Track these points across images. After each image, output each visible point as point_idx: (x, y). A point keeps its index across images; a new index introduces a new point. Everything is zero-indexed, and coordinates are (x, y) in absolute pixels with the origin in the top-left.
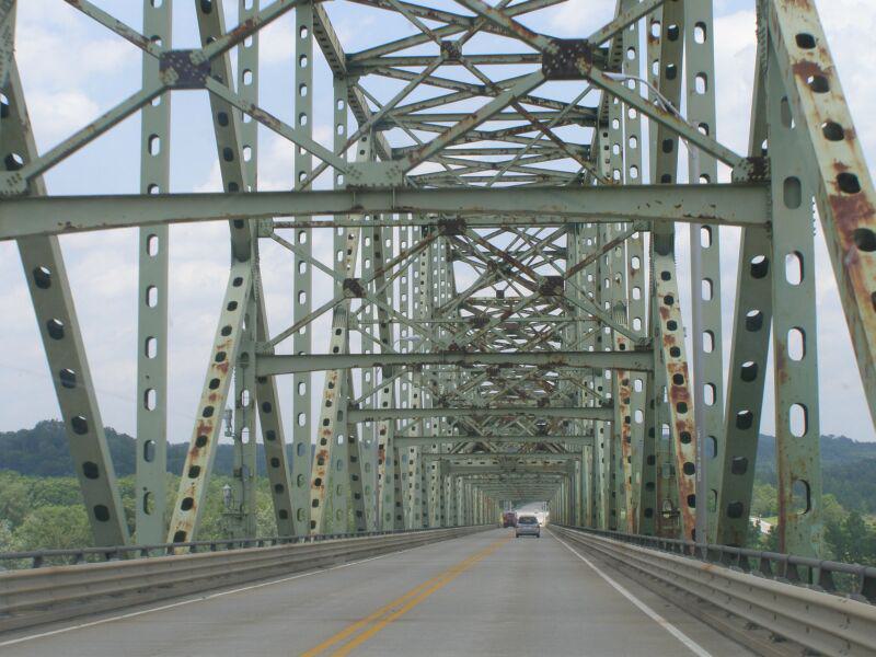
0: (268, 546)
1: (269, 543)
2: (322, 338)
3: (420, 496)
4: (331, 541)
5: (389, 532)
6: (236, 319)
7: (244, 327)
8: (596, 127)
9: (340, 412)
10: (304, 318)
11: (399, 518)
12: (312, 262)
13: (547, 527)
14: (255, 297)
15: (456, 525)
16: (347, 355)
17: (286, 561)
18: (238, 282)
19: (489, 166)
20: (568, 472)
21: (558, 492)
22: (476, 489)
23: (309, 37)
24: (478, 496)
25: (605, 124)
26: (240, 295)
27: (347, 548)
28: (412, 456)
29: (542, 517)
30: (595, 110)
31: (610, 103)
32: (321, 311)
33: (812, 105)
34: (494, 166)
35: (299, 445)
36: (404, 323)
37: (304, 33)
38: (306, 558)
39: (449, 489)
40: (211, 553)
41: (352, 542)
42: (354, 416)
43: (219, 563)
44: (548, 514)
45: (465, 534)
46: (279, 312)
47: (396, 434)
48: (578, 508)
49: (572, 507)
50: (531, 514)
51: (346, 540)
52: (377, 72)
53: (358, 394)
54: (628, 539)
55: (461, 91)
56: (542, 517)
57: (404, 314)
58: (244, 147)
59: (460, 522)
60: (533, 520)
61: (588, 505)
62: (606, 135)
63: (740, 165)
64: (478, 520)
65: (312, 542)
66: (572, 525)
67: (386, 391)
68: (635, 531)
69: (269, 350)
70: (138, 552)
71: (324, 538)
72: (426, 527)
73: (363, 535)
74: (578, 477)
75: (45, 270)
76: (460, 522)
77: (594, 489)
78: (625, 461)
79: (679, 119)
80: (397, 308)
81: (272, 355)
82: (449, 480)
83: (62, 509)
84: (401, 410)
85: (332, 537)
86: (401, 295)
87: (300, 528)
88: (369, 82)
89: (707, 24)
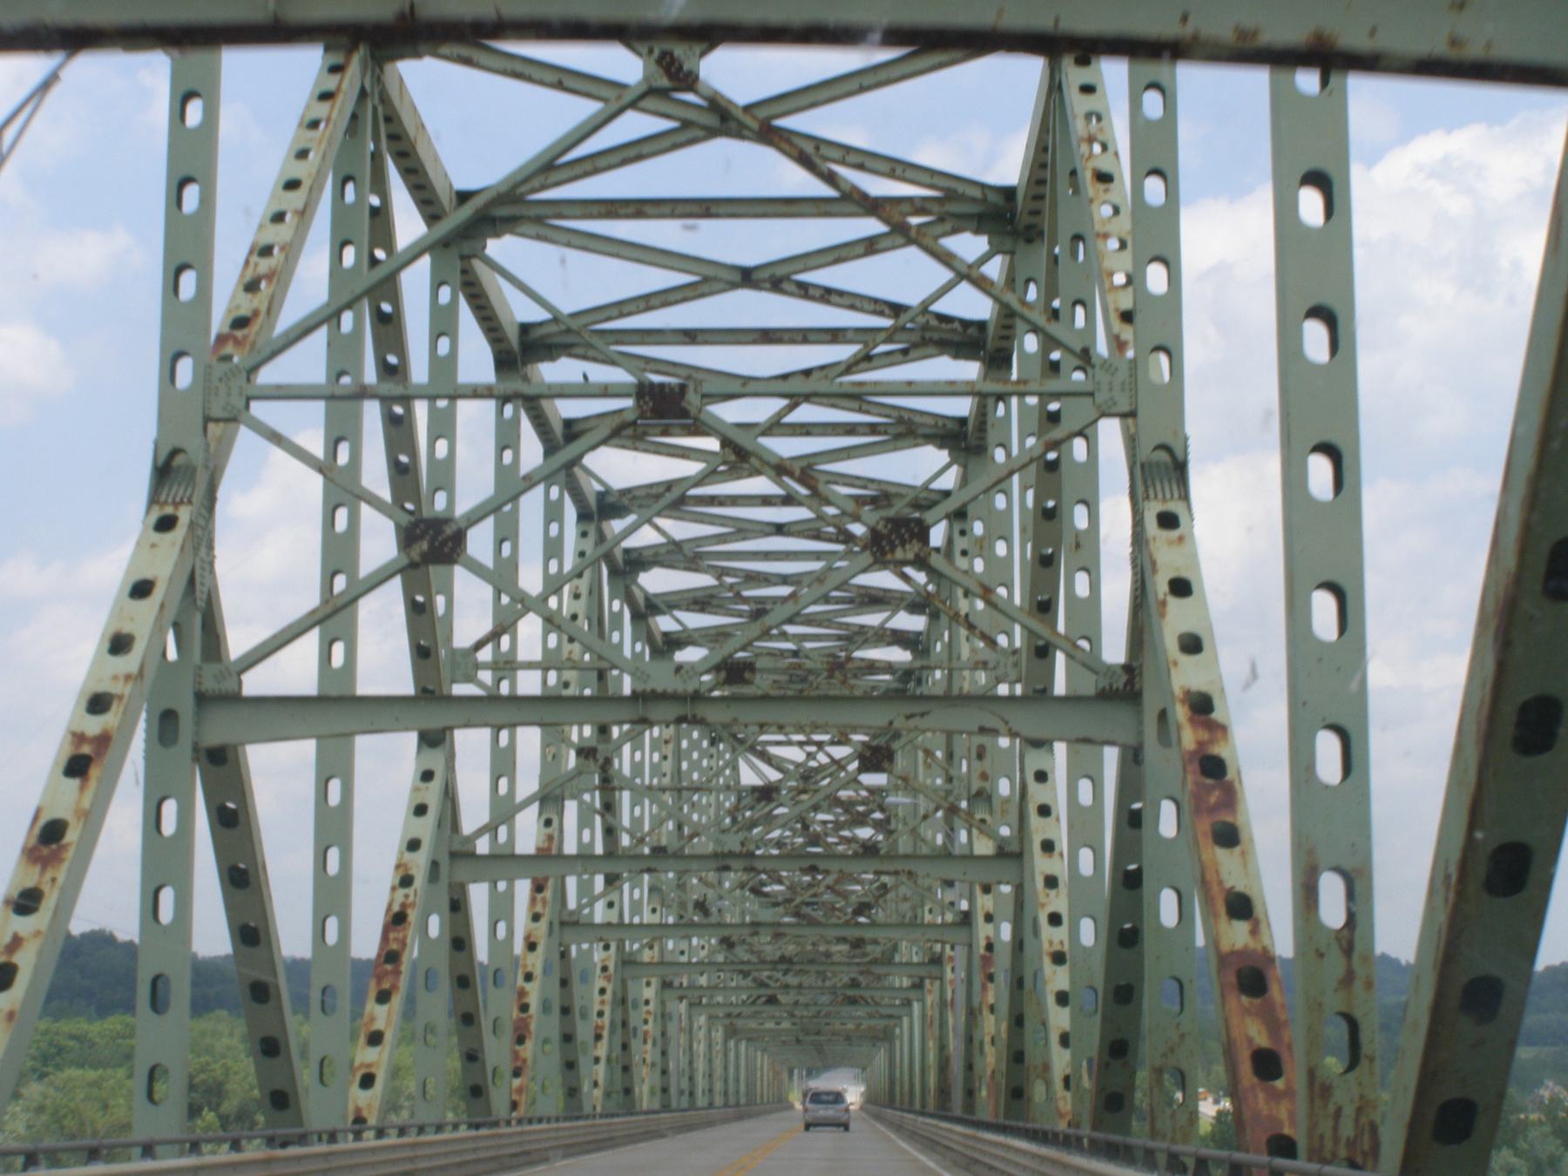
0: (463, 1132)
1: (394, 1132)
2: (527, 833)
3: (658, 1059)
4: (544, 1126)
5: (654, 1112)
6: (425, 828)
7: (172, 654)
8: (983, 360)
9: (435, 865)
10: (504, 810)
11: (628, 1091)
12: (325, 468)
13: (862, 1108)
14: (450, 795)
15: (711, 1105)
16: (560, 856)
17: (590, 1138)
18: (427, 776)
19: (772, 529)
20: (885, 1037)
21: (877, 1058)
22: (759, 1053)
23: (454, 300)
24: (763, 1061)
25: (997, 360)
26: (432, 794)
27: (475, 1150)
28: (649, 993)
29: (854, 1095)
30: (1009, 193)
31: (990, 415)
32: (527, 803)
33: (1177, 618)
34: (784, 580)
35: (427, 972)
36: (639, 794)
37: (445, 294)
38: (581, 1131)
39: (732, 1055)
40: (235, 1157)
41: (558, 1129)
42: (462, 870)
43: (365, 1160)
44: (863, 1089)
45: (750, 1116)
46: (474, 812)
47: (566, 918)
48: (898, 1084)
49: (892, 1082)
50: (839, 1088)
51: (519, 1129)
52: (571, 355)
53: (572, 904)
54: (1068, 1142)
55: (740, 531)
56: (854, 1095)
57: (638, 781)
58: (438, 593)
59: (743, 1101)
60: (838, 1097)
61: (906, 1078)
62: (963, 533)
63: (1105, 674)
64: (762, 1097)
65: (392, 1139)
66: (891, 1103)
67: (611, 905)
68: (996, 1116)
69: (228, 686)
70: (138, 1151)
71: (530, 1121)
72: (666, 1107)
73: (578, 1118)
74: (898, 1043)
75: (231, 805)
76: (743, 1101)
77: (911, 1069)
78: (986, 1012)
79: (1024, 627)
80: (627, 771)
81: (235, 698)
82: (732, 1043)
83: (92, 1074)
84: (631, 925)
85: (540, 1120)
86: (435, 336)
87: (317, 1108)
88: (558, 371)
89: (1170, 258)
